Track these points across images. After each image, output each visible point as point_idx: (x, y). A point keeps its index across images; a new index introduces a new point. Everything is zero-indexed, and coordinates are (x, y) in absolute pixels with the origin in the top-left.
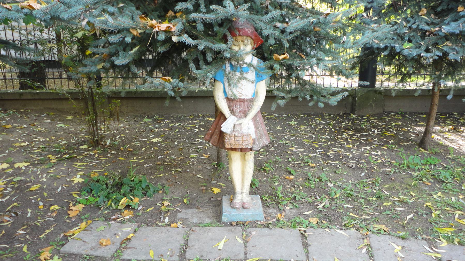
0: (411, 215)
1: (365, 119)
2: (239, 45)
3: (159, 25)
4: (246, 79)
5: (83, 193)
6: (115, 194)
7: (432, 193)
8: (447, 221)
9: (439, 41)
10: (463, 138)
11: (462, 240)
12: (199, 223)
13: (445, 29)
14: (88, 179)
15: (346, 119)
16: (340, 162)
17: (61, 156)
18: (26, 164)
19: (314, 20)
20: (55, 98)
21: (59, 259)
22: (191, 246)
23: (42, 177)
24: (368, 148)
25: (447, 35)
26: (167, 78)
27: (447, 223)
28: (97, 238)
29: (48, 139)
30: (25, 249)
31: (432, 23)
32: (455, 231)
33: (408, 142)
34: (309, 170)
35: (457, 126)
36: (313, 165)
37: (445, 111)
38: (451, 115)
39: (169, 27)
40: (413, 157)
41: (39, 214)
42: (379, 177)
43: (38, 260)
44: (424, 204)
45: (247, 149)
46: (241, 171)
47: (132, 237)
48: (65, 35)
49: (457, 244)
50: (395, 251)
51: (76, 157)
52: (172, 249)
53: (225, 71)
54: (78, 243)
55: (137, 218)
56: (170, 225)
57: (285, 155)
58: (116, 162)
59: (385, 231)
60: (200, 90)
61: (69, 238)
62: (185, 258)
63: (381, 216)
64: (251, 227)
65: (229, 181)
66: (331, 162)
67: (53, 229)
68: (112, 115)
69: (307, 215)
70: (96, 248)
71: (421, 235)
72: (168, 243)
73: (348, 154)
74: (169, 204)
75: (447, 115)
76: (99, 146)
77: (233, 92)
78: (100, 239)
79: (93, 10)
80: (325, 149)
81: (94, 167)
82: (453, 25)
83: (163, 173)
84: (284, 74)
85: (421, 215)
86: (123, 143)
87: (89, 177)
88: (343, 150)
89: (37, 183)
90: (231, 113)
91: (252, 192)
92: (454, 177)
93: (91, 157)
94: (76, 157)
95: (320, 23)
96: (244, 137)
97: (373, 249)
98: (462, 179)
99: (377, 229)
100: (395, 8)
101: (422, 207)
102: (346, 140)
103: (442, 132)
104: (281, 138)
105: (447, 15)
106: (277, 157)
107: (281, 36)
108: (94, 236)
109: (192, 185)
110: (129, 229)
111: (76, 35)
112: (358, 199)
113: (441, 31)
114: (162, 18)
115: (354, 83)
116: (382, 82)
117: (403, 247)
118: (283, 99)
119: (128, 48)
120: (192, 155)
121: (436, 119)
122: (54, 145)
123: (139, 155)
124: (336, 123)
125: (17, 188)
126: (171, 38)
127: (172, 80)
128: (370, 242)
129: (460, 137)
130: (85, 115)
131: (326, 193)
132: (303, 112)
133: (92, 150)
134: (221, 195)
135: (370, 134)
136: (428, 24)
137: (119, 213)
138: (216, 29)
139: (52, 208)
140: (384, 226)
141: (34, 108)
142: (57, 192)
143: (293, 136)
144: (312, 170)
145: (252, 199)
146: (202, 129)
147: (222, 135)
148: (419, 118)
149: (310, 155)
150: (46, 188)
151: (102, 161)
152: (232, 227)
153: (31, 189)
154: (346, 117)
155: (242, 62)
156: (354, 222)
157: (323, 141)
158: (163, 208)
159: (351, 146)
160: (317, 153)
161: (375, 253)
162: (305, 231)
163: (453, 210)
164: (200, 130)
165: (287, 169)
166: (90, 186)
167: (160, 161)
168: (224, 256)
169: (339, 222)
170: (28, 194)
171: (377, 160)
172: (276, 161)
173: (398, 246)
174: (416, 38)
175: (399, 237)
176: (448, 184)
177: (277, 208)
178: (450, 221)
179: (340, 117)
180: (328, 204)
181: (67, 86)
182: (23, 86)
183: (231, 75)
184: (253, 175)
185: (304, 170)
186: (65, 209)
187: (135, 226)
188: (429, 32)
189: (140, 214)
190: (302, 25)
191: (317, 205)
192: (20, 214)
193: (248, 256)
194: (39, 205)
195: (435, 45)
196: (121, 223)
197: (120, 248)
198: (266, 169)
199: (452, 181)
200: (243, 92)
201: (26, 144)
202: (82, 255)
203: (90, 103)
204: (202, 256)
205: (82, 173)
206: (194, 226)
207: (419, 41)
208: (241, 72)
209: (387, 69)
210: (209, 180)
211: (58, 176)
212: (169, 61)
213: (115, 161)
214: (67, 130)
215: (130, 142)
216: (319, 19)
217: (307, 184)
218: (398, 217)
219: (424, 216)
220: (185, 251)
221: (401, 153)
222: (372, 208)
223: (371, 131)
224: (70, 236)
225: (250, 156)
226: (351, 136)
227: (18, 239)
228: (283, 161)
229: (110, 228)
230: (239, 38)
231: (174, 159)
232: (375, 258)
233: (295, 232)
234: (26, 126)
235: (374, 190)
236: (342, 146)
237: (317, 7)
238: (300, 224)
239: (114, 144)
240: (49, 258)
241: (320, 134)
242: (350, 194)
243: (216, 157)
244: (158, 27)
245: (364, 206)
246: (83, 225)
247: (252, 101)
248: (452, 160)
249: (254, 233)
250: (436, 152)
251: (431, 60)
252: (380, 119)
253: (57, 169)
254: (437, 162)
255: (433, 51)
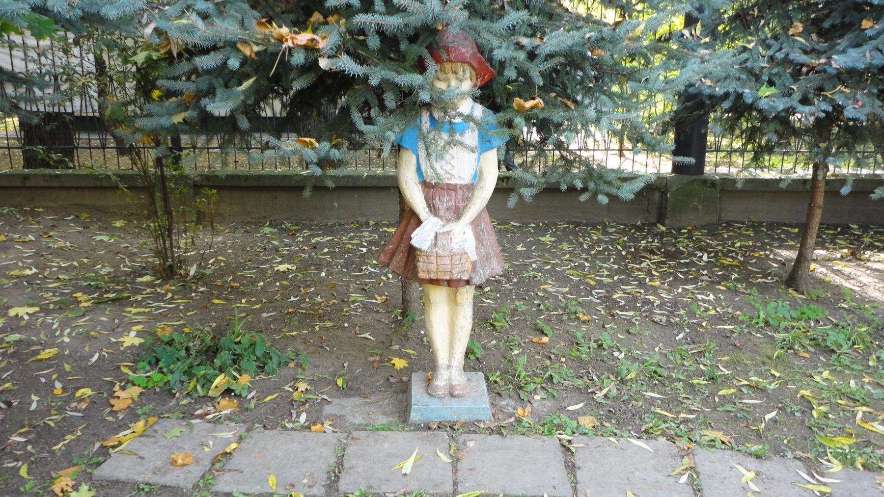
0: (773, 414)
1: (684, 233)
2: (447, 80)
3: (293, 35)
4: (460, 144)
5: (141, 365)
6: (203, 367)
7: (812, 372)
8: (840, 426)
9: (827, 85)
10: (868, 272)
11: (871, 460)
12: (366, 425)
13: (839, 61)
14: (150, 340)
15: (648, 233)
16: (638, 313)
17: (101, 295)
18: (31, 310)
19: (592, 33)
20: (91, 185)
21: (89, 490)
22: (350, 468)
23: (62, 335)
24: (689, 287)
25: (842, 73)
26: (307, 140)
27: (842, 429)
28: (166, 451)
29: (75, 263)
30: (23, 472)
31: (813, 50)
32: (857, 444)
33: (765, 277)
34: (578, 328)
35: (858, 249)
36: (585, 318)
37: (836, 221)
38: (846, 230)
39: (313, 40)
40: (776, 304)
41: (54, 404)
42: (710, 341)
43: (48, 492)
44: (797, 392)
45: (460, 280)
46: (449, 325)
47: (234, 450)
48: (113, 62)
49: (862, 469)
50: (744, 480)
51: (129, 297)
52: (311, 474)
53: (420, 129)
54: (129, 461)
55: (246, 413)
56: (310, 428)
57: (532, 299)
58: (206, 307)
59: (723, 442)
60: (371, 173)
61: (111, 451)
62: (338, 491)
63: (715, 415)
64: (466, 433)
65: (424, 346)
66: (620, 313)
67: (79, 433)
68: (200, 219)
69: (574, 411)
70: (163, 470)
71: (793, 451)
72: (304, 462)
73: (652, 298)
74: (309, 388)
75: (839, 229)
76: (175, 277)
77: (435, 171)
78: (173, 453)
79: (167, 8)
80: (609, 289)
81: (163, 316)
82: (854, 54)
83: (297, 328)
84: (535, 137)
85: (793, 413)
86: (221, 273)
87: (153, 334)
88: (642, 291)
89: (51, 346)
90: (430, 211)
91: (469, 367)
92: (854, 344)
93: (159, 297)
94: (129, 297)
95: (603, 39)
96: (454, 257)
97: (701, 477)
98: (868, 347)
99: (707, 438)
100: (743, 21)
101: (793, 399)
102: (649, 273)
103: (830, 260)
104: (525, 266)
105: (841, 36)
106: (517, 303)
107: (528, 65)
108: (160, 447)
109: (354, 353)
110: (230, 435)
111: (135, 58)
112: (671, 383)
113: (831, 65)
114: (300, 25)
115: (659, 165)
116: (716, 166)
117: (758, 473)
118: (531, 186)
119: (234, 81)
120: (354, 296)
121: (819, 236)
122: (87, 275)
123: (251, 294)
124: (630, 240)
125: (13, 355)
126: (316, 61)
127: (317, 145)
128: (695, 463)
129: (863, 270)
130: (148, 218)
131: (611, 370)
132: (567, 220)
133: (160, 285)
134: (408, 371)
135: (693, 261)
136: (805, 52)
137: (210, 404)
138: (403, 46)
139: (78, 394)
140: (721, 433)
141: (51, 205)
142: (90, 364)
143: (548, 264)
144: (584, 328)
145: (469, 380)
146: (373, 248)
147: (412, 253)
148: (786, 233)
149: (580, 299)
150: (70, 355)
151: (179, 306)
152: (429, 432)
153: (39, 357)
154: (649, 230)
155: (452, 113)
156: (664, 426)
157: (605, 273)
158: (296, 396)
159: (657, 283)
160: (592, 295)
161: (705, 483)
162: (570, 442)
163: (851, 404)
164: (370, 250)
165: (536, 325)
166: (155, 352)
167: (292, 307)
168: (413, 486)
169: (636, 425)
170: (33, 367)
171: (707, 310)
172: (515, 310)
173: (749, 471)
174: (783, 78)
175: (750, 454)
176: (842, 356)
177: (516, 397)
178: (847, 425)
179: (637, 230)
180: (615, 391)
181: (114, 164)
182: (30, 161)
183: (431, 136)
184: (471, 335)
185: (568, 328)
186: (105, 395)
187: (241, 429)
188: (808, 66)
189: (252, 405)
190: (569, 43)
191: (594, 393)
192: (15, 404)
193: (460, 488)
194: (54, 387)
195: (820, 89)
196: (214, 422)
197: (210, 470)
198: (496, 324)
199: (849, 351)
200: (453, 170)
201: (32, 272)
202: (134, 484)
203: (158, 195)
204: (370, 487)
205: (139, 327)
206: (356, 430)
207: (788, 84)
208: (452, 132)
209: (725, 142)
210: (386, 344)
211: (93, 333)
212: (313, 112)
213: (204, 306)
214: (113, 248)
215: (235, 271)
216: (601, 31)
217: (575, 353)
218: (749, 417)
219: (798, 414)
220: (338, 477)
221: (752, 297)
222: (698, 399)
223: (695, 256)
224: (113, 447)
225: (467, 295)
226: (658, 264)
227: (11, 452)
228: (528, 310)
229: (191, 432)
230: (448, 66)
231: (319, 304)
232: (706, 492)
233: (551, 444)
234: (33, 238)
235: (701, 366)
236: (641, 284)
237: (596, 14)
238: (561, 427)
239: (204, 274)
240: (70, 490)
241: (600, 260)
242: (656, 372)
243: (400, 301)
244: (292, 39)
245: (684, 395)
246: (140, 425)
247: (470, 188)
248: (849, 311)
249: (471, 444)
250: (818, 297)
251: (812, 119)
252: (713, 233)
253: (91, 320)
254: (821, 315)
255: (816, 102)
